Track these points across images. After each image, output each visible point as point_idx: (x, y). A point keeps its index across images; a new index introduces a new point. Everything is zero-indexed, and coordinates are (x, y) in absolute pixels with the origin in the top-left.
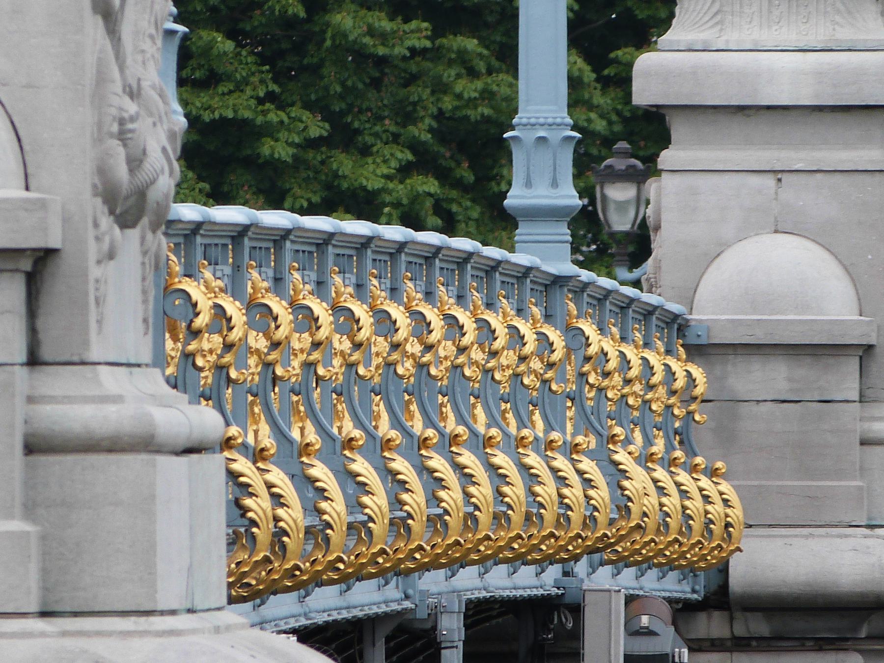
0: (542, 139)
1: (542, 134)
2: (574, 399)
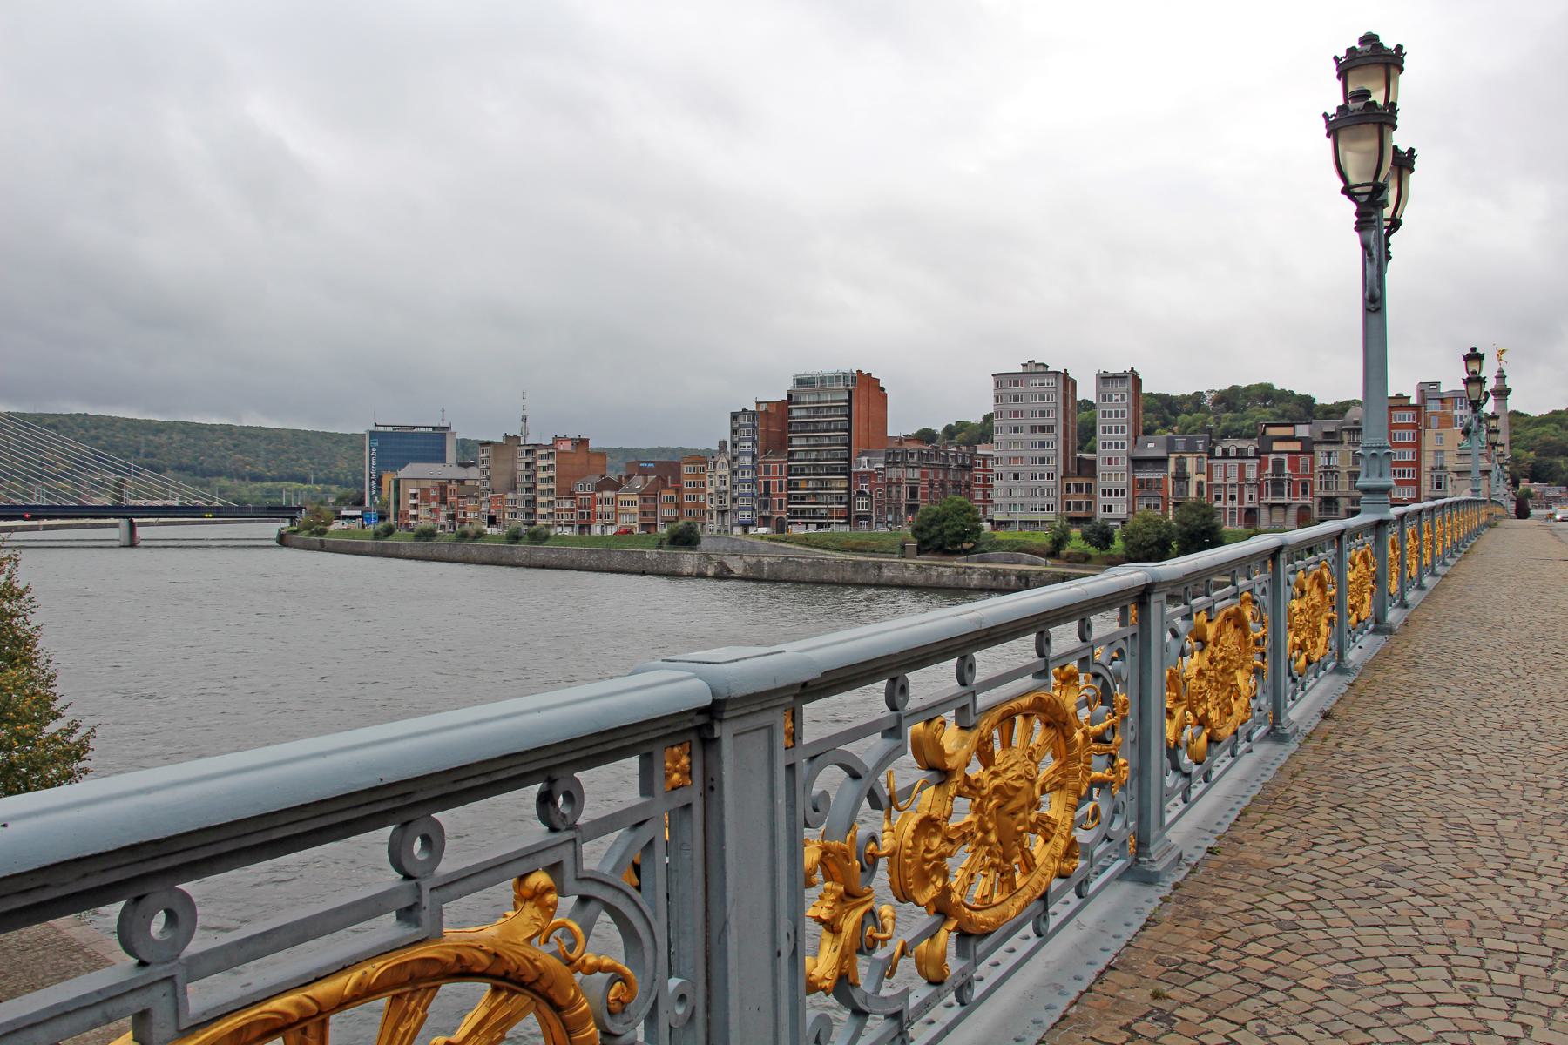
0: (1374, 455)
1: (1374, 451)
2: (1218, 742)
